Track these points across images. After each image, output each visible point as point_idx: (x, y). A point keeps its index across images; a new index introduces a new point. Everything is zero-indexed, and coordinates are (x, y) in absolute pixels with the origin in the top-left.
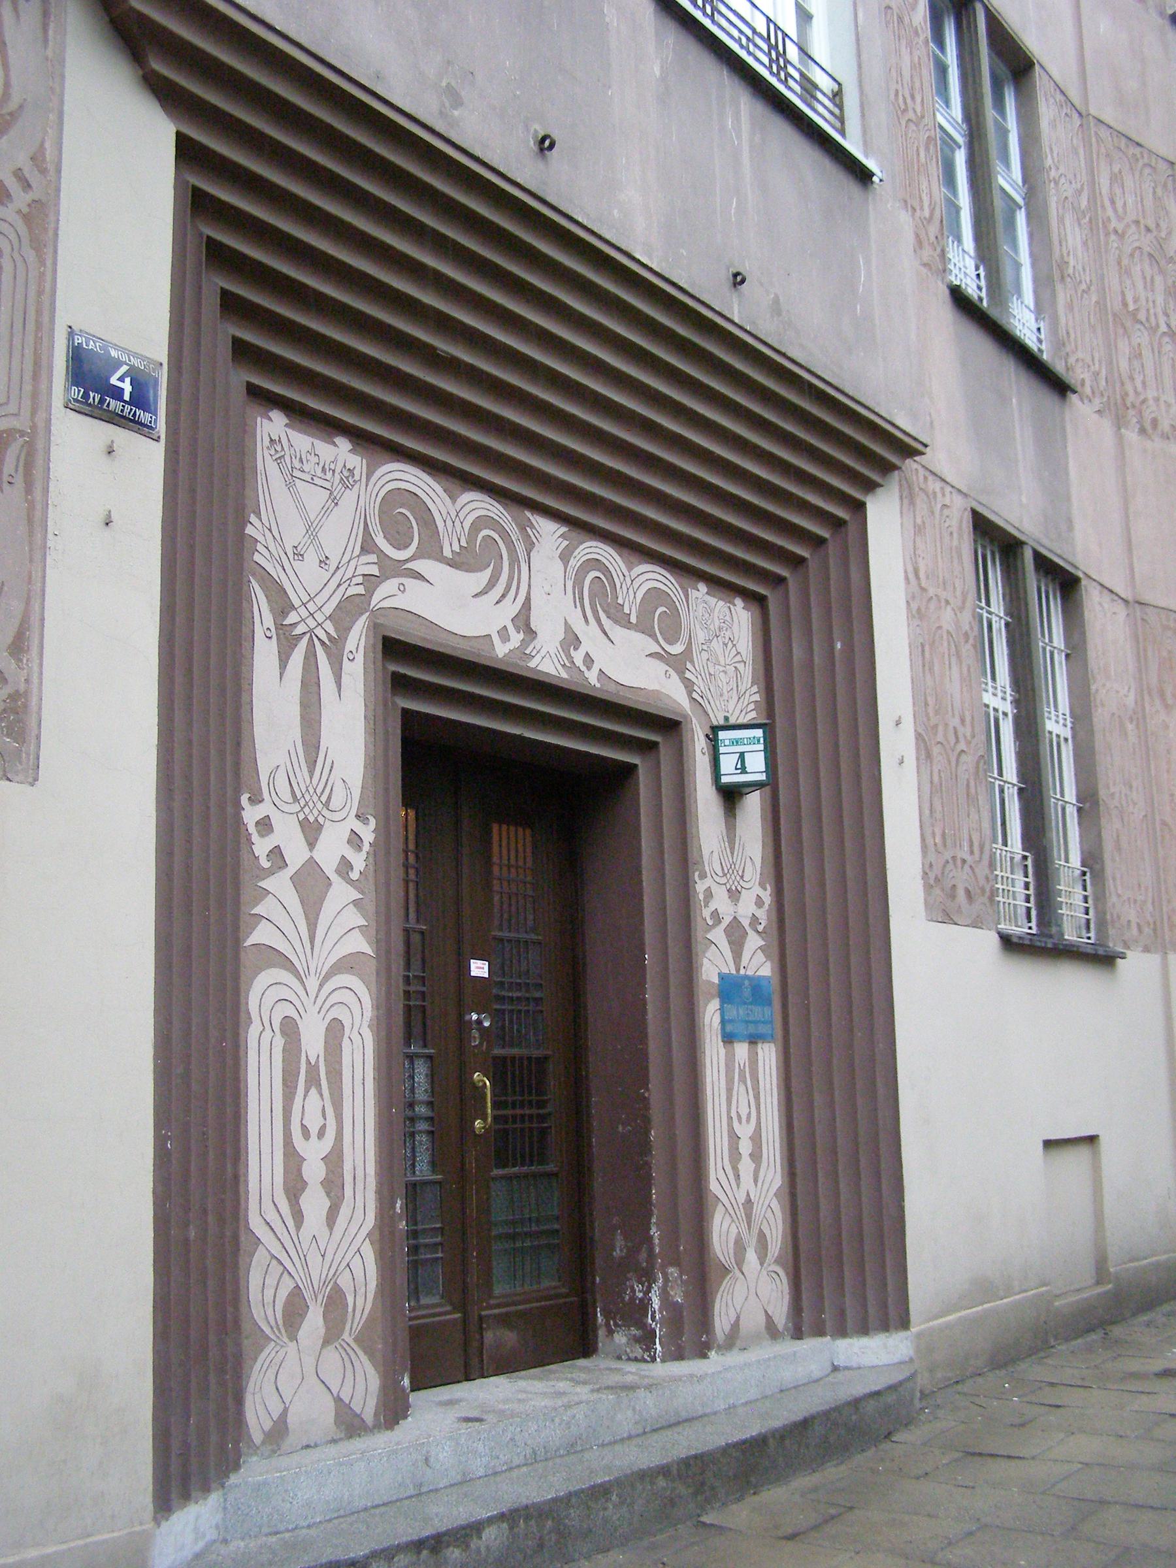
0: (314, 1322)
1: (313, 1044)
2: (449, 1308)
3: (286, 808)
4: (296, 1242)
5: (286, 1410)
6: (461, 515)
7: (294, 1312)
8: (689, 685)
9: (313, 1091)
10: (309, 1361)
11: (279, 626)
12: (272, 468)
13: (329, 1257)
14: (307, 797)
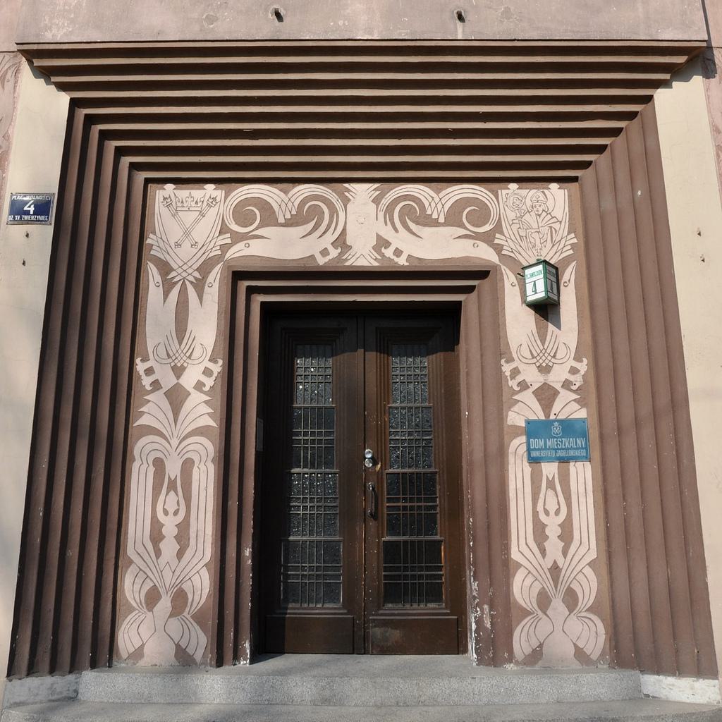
0: (165, 604)
1: (173, 469)
2: (346, 611)
3: (163, 361)
4: (156, 564)
5: (143, 645)
6: (292, 200)
7: (152, 598)
8: (498, 249)
9: (172, 493)
10: (160, 623)
11: (164, 280)
12: (164, 210)
13: (177, 574)
14: (177, 355)
